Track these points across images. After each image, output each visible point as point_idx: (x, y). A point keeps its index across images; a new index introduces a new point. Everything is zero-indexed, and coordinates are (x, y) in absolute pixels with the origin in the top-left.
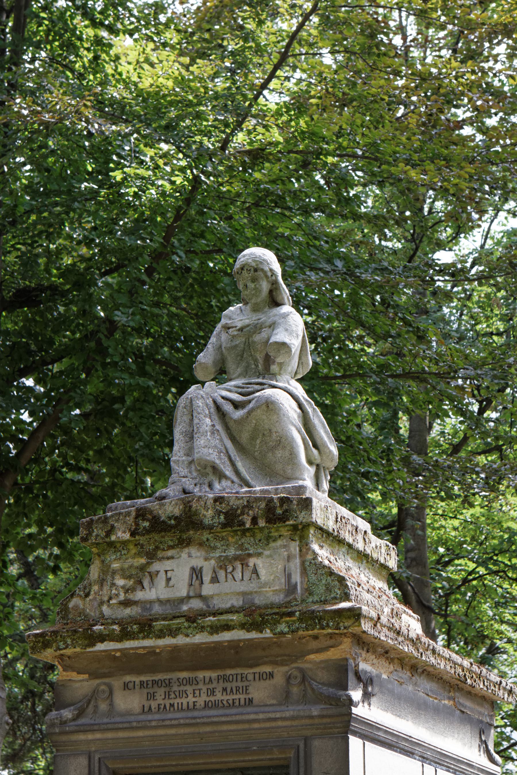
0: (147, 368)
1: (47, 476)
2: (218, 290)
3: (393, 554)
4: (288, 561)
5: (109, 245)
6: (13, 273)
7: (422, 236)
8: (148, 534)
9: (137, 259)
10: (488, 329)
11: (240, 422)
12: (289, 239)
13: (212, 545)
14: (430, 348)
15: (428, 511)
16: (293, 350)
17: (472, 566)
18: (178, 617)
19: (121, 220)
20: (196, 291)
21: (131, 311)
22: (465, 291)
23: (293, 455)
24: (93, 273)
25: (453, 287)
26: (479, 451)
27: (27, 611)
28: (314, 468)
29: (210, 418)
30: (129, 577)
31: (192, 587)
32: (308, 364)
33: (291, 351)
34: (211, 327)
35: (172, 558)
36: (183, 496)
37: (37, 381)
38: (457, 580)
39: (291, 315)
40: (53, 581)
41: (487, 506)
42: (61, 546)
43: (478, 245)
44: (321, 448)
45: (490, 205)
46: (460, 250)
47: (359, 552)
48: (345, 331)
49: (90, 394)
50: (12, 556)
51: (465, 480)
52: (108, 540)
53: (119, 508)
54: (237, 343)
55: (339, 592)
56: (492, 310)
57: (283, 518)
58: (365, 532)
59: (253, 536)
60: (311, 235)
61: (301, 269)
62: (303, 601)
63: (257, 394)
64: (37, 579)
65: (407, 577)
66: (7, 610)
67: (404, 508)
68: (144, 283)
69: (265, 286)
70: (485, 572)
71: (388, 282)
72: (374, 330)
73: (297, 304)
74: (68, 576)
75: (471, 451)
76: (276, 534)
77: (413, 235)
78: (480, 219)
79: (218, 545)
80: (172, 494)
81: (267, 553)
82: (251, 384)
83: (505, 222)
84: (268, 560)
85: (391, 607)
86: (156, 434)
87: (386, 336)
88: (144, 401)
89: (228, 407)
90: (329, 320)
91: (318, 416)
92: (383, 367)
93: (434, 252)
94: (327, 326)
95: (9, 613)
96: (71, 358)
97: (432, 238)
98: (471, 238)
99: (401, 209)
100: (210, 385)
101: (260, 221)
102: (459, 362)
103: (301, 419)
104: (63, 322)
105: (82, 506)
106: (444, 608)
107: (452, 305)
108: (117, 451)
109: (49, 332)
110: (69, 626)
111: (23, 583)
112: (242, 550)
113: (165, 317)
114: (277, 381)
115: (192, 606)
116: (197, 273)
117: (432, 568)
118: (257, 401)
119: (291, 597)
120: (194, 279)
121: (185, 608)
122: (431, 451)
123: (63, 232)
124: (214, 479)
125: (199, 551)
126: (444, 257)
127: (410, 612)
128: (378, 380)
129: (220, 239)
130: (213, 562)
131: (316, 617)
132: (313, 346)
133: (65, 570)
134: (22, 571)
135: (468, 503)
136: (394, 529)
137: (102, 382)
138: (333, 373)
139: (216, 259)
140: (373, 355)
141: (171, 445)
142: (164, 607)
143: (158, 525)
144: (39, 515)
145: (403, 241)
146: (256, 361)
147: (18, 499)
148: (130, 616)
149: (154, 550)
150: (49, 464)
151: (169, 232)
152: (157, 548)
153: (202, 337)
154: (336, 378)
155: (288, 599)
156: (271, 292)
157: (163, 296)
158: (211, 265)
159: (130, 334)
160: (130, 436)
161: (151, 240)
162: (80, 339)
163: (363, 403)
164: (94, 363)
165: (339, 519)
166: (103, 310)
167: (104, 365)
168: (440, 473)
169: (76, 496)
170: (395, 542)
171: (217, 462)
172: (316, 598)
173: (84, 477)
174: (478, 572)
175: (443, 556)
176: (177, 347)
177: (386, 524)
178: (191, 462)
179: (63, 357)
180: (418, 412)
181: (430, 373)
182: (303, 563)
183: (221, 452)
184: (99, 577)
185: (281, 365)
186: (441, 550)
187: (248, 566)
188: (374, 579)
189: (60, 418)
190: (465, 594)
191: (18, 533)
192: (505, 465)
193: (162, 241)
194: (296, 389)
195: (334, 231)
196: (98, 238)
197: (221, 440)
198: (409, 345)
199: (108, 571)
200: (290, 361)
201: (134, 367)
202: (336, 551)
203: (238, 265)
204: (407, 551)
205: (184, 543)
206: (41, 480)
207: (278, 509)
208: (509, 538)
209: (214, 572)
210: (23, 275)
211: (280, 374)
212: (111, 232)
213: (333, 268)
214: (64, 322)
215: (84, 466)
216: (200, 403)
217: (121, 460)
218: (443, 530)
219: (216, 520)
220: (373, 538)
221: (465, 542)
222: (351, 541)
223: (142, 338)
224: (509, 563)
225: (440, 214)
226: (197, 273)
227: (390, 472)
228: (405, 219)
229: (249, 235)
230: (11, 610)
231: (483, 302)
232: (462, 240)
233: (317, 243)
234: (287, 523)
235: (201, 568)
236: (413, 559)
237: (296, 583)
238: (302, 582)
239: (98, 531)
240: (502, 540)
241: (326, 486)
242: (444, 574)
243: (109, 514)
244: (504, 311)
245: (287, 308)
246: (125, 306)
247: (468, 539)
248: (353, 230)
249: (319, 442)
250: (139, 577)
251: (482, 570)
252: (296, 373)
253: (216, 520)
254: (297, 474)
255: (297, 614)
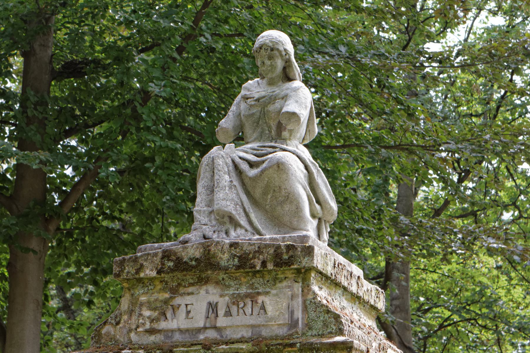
0: (175, 133)
1: (85, 223)
2: (238, 68)
3: (382, 297)
4: (292, 300)
5: (145, 27)
6: (62, 48)
7: (414, 29)
8: (172, 273)
9: (170, 39)
10: (468, 111)
11: (255, 179)
12: (301, 27)
13: (227, 284)
14: (418, 124)
15: (411, 265)
16: (302, 120)
17: (447, 313)
18: (196, 344)
19: (157, 5)
20: (219, 69)
21: (163, 83)
22: (449, 77)
23: (298, 209)
24: (130, 51)
25: (439, 74)
26: (457, 215)
27: (64, 339)
28: (317, 220)
29: (229, 175)
30: (155, 309)
31: (208, 319)
32: (314, 131)
33: (300, 120)
34: (231, 100)
35: (192, 293)
36: (204, 241)
37: (81, 141)
38: (434, 326)
39: (301, 89)
40: (87, 315)
41: (462, 263)
42: (95, 283)
43: (462, 38)
44: (323, 204)
45: (474, 5)
46: (446, 43)
47: (352, 294)
48: (346, 108)
49: (125, 154)
50: (53, 292)
51: (443, 239)
52: (137, 276)
53: (148, 249)
54: (254, 111)
55: (334, 328)
56: (472, 95)
57: (288, 263)
58: (359, 277)
59: (263, 277)
60: (320, 24)
61: (310, 52)
62: (303, 334)
63: (270, 156)
64: (73, 312)
65: (392, 321)
66: (47, 337)
67: (391, 262)
68: (174, 60)
69: (280, 64)
70: (459, 320)
71: (384, 66)
72: (371, 107)
73: (306, 82)
74: (100, 311)
75: (450, 216)
76: (282, 276)
77: (407, 28)
78: (465, 16)
79: (232, 283)
80: (193, 239)
81: (274, 292)
82: (264, 147)
83: (486, 20)
84: (274, 298)
85: (378, 342)
86: (180, 190)
87: (381, 113)
88: (171, 161)
89: (244, 166)
90: (332, 98)
91: (321, 177)
92: (377, 140)
93: (425, 43)
94: (331, 104)
95: (49, 340)
96: (109, 122)
97: (423, 31)
98: (456, 33)
99: (397, 5)
100: (230, 146)
101: (276, 10)
102: (443, 137)
103: (306, 179)
104: (104, 91)
105: (116, 249)
106: (422, 349)
107: (438, 89)
108: (146, 204)
109: (91, 100)
110: (101, 349)
111: (62, 315)
112: (252, 289)
113: (192, 90)
114: (287, 145)
115: (208, 335)
116: (221, 53)
117: (413, 314)
118: (269, 162)
119: (293, 331)
120: (218, 58)
121: (202, 337)
122: (416, 215)
123: (107, 15)
124: (230, 227)
125: (215, 288)
126: (432, 47)
127: (395, 347)
128: (373, 150)
129: (242, 25)
130: (227, 298)
131: (314, 348)
132: (318, 119)
133: (98, 306)
134: (60, 305)
135: (446, 260)
136: (383, 279)
137: (136, 144)
138: (334, 143)
139: (237, 42)
140: (370, 130)
141: (193, 199)
142: (183, 336)
143: (181, 265)
144: (78, 257)
145: (398, 33)
146: (270, 127)
147: (60, 242)
148: (154, 343)
149: (177, 286)
150: (88, 213)
151: (198, 17)
152: (179, 285)
153: (224, 109)
154: (336, 147)
155: (291, 332)
156: (284, 68)
157: (190, 72)
158: (233, 47)
159: (162, 103)
160: (158, 191)
161: (182, 23)
162: (118, 106)
163: (359, 170)
164: (129, 127)
165: (336, 266)
166: (139, 82)
167: (138, 129)
168: (423, 231)
169: (109, 241)
170: (384, 287)
171: (234, 212)
172: (314, 332)
173: (117, 225)
174: (453, 319)
175: (423, 304)
176: (202, 116)
177: (376, 275)
178: (211, 212)
179: (102, 122)
180: (406, 180)
181: (418, 146)
182: (304, 302)
183: (237, 204)
184: (129, 308)
185: (291, 131)
186: (422, 299)
187: (257, 303)
188: (365, 318)
189: (99, 173)
190: (441, 338)
191: (58, 271)
192: (479, 227)
193: (192, 24)
194: (304, 152)
195: (340, 23)
196: (137, 20)
197: (238, 194)
198: (402, 120)
199: (136, 303)
200: (299, 128)
201: (164, 131)
202: (333, 293)
203: (257, 45)
204: (393, 299)
205: (202, 281)
206: (81, 226)
207: (285, 254)
208: (481, 291)
209: (228, 307)
210: (70, 50)
211: (290, 139)
212: (148, 16)
213: (338, 52)
214: (105, 91)
215: (118, 216)
216: (220, 162)
217: (150, 212)
218: (424, 282)
219: (231, 262)
220: (365, 282)
221: (442, 293)
222: (346, 284)
223: (171, 108)
224: (479, 313)
225: (431, 11)
226: (221, 53)
227: (380, 229)
228: (401, 14)
229: (266, 22)
230: (50, 338)
231: (465, 88)
232: (449, 34)
233: (325, 31)
234: (292, 267)
235: (217, 303)
236: (397, 307)
237: (298, 319)
238: (303, 318)
239: (129, 269)
240: (474, 292)
241: (326, 236)
242: (423, 320)
243: (139, 254)
244: (482, 96)
245: (298, 83)
246: (158, 79)
247: (445, 290)
248: (355, 22)
249: (321, 199)
250: (163, 310)
251: (456, 318)
252: (304, 139)
253: (231, 262)
254: (302, 226)
255: (298, 345)
